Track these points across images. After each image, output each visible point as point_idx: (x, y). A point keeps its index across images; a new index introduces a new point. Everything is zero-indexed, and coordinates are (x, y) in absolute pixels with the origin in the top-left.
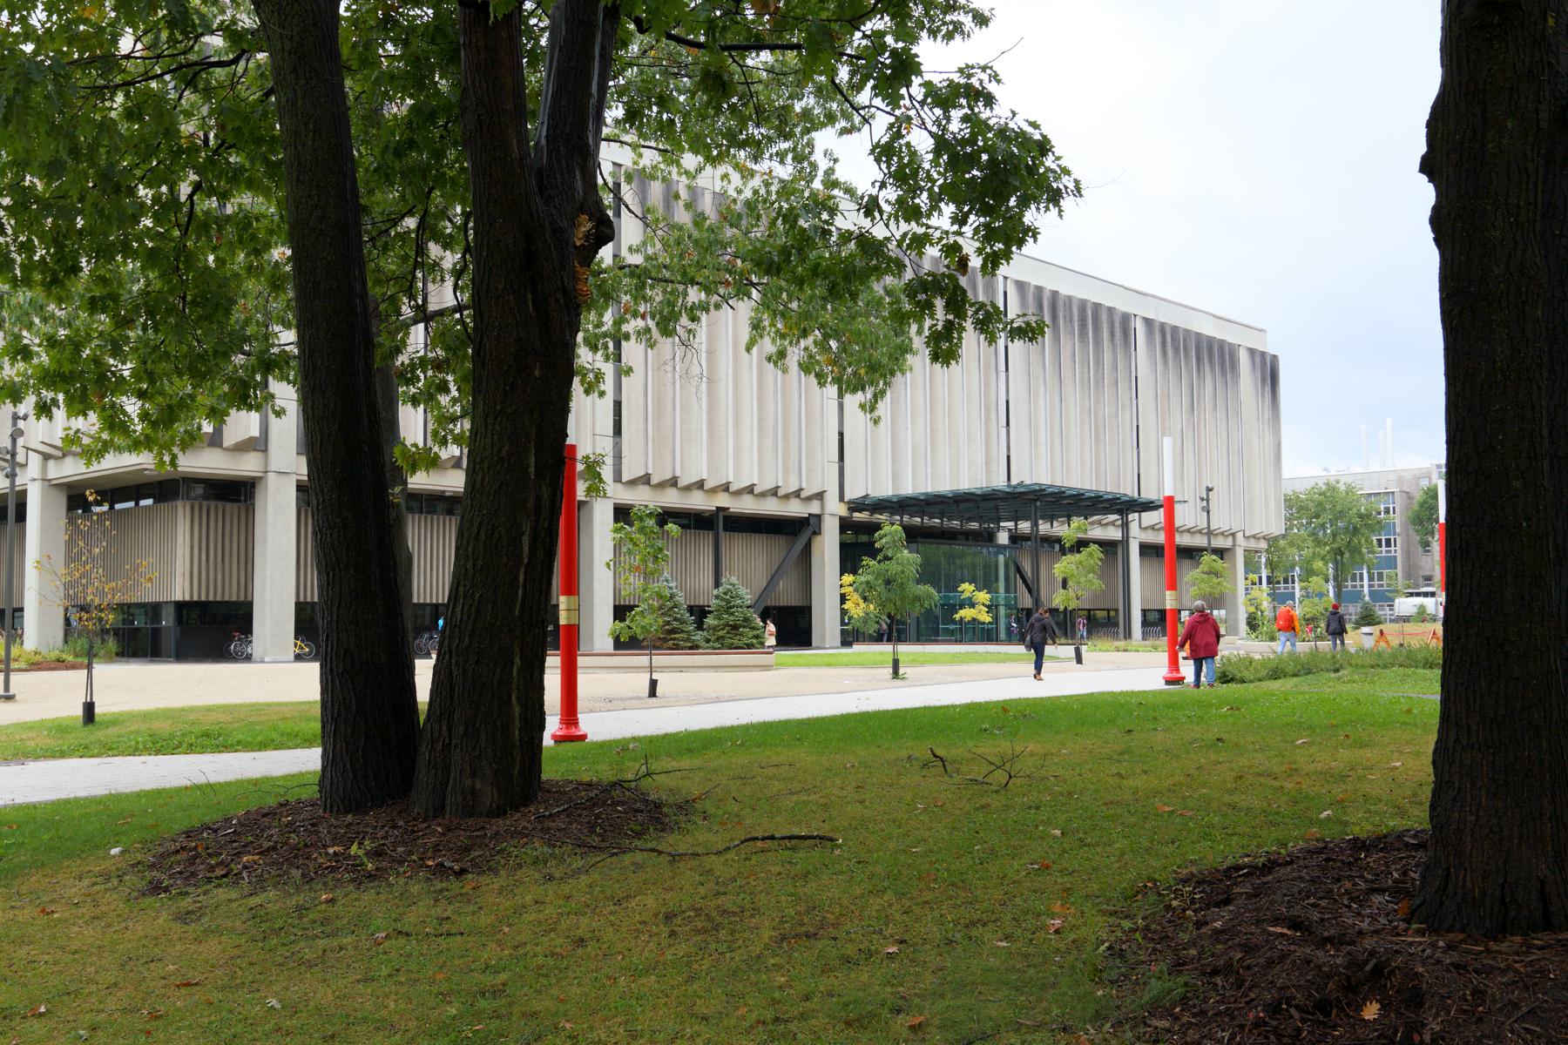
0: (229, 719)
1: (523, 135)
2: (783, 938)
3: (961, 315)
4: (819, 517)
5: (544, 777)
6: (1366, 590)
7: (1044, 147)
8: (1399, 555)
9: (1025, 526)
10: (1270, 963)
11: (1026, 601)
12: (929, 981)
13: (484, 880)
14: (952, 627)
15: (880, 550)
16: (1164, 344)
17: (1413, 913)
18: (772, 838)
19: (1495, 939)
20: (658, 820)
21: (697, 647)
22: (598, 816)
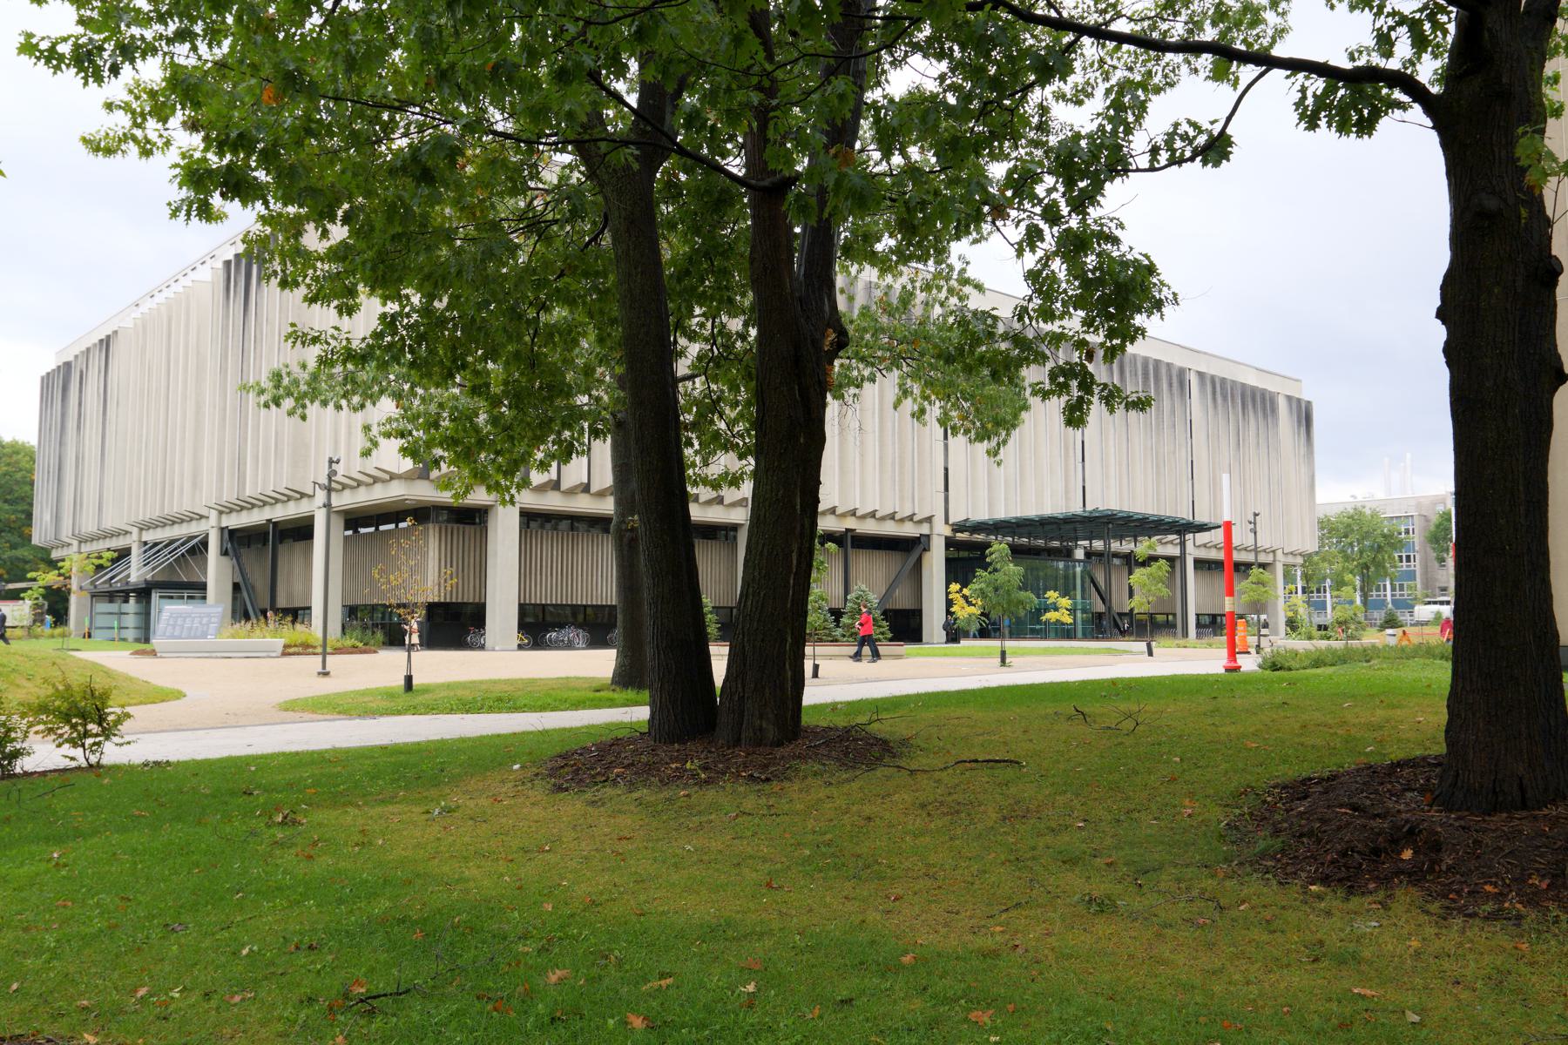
0: (512, 688)
1: (232, 47)
2: (1004, 818)
3: (1090, 392)
4: (928, 537)
5: (803, 723)
6: (1389, 598)
7: (1151, 269)
8: (1418, 569)
9: (1098, 545)
10: (1340, 828)
11: (1100, 607)
12: (1109, 841)
13: (786, 784)
14: (1038, 627)
15: (990, 564)
16: (1214, 393)
17: (1434, 799)
18: (976, 761)
19: (1489, 815)
20: (889, 751)
21: (836, 641)
22: (847, 748)
